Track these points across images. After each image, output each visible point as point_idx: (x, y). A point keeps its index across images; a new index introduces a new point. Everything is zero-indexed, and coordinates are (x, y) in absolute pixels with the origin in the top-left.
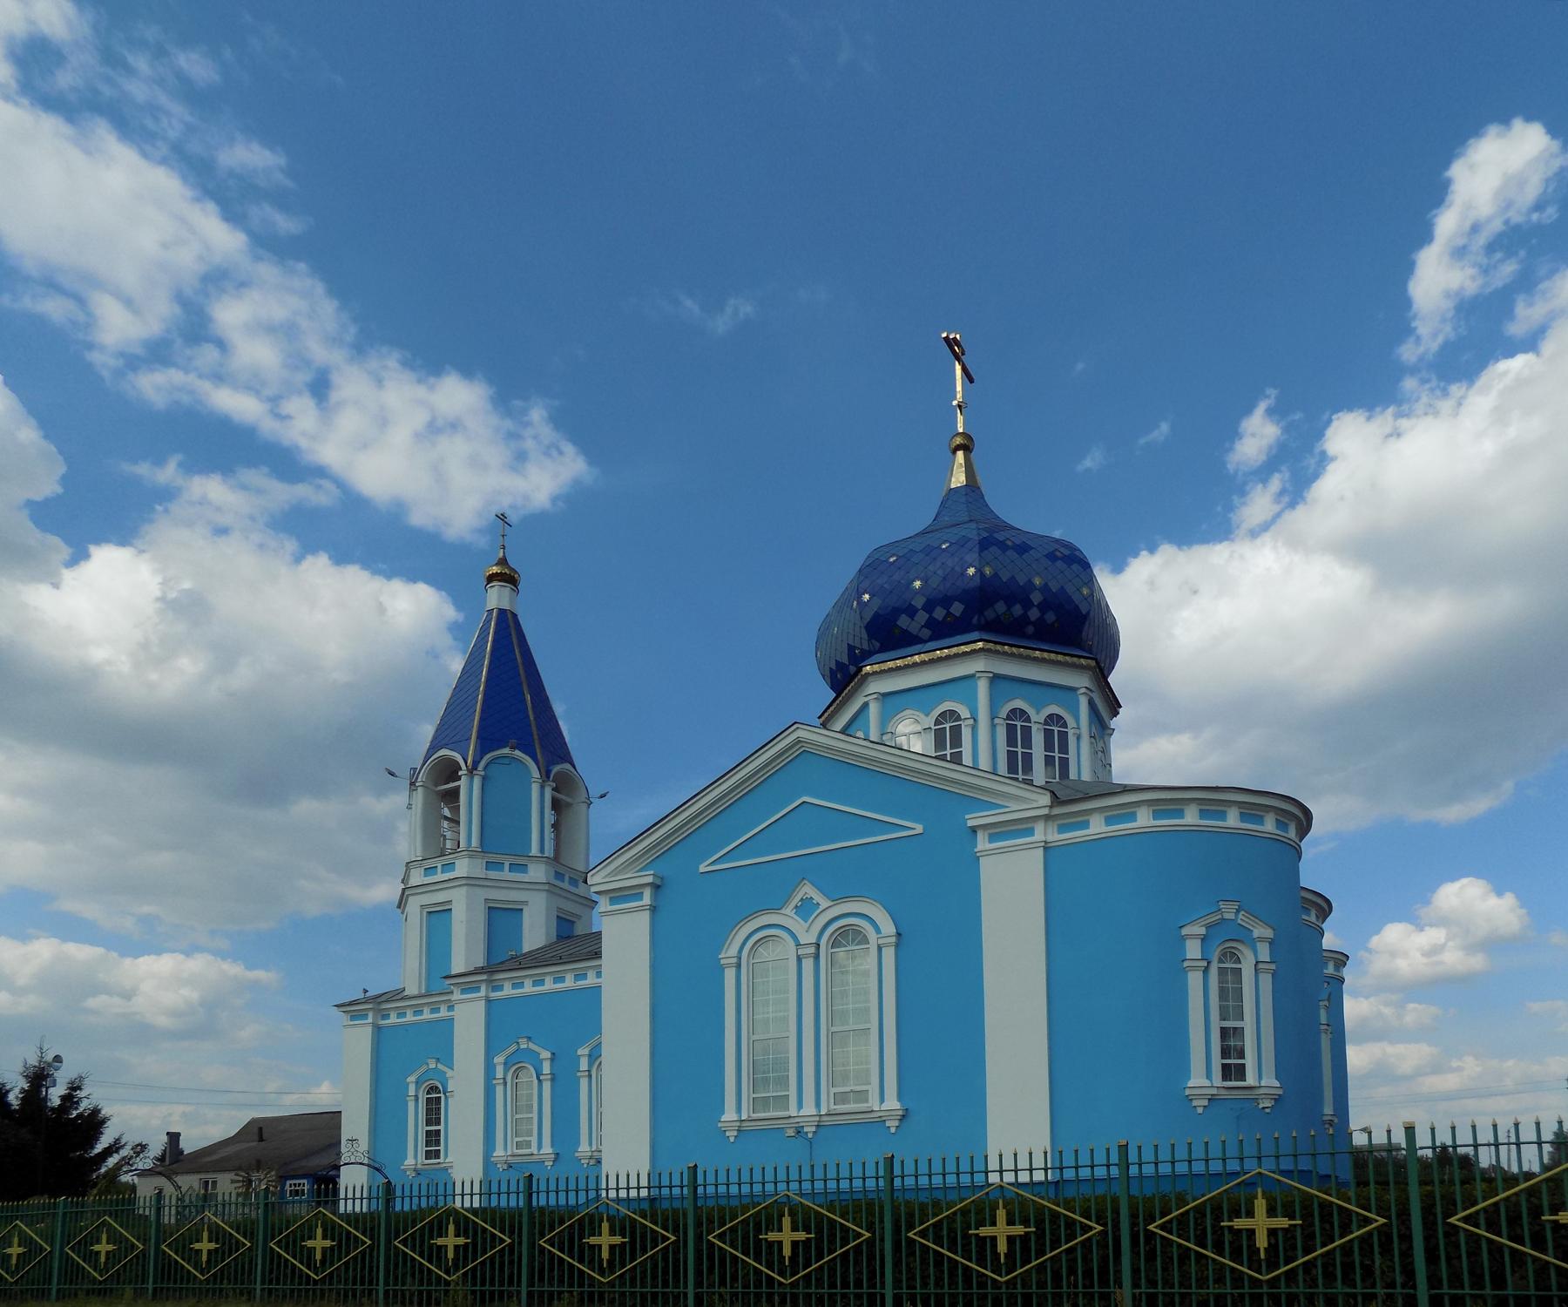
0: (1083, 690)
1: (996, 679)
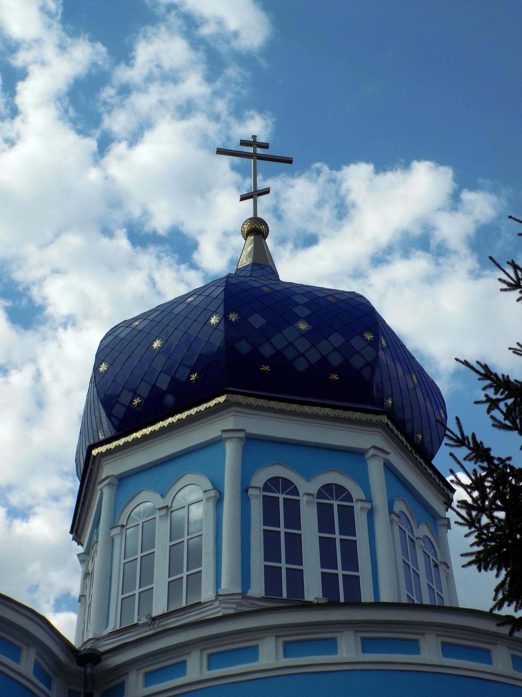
0: (372, 452)
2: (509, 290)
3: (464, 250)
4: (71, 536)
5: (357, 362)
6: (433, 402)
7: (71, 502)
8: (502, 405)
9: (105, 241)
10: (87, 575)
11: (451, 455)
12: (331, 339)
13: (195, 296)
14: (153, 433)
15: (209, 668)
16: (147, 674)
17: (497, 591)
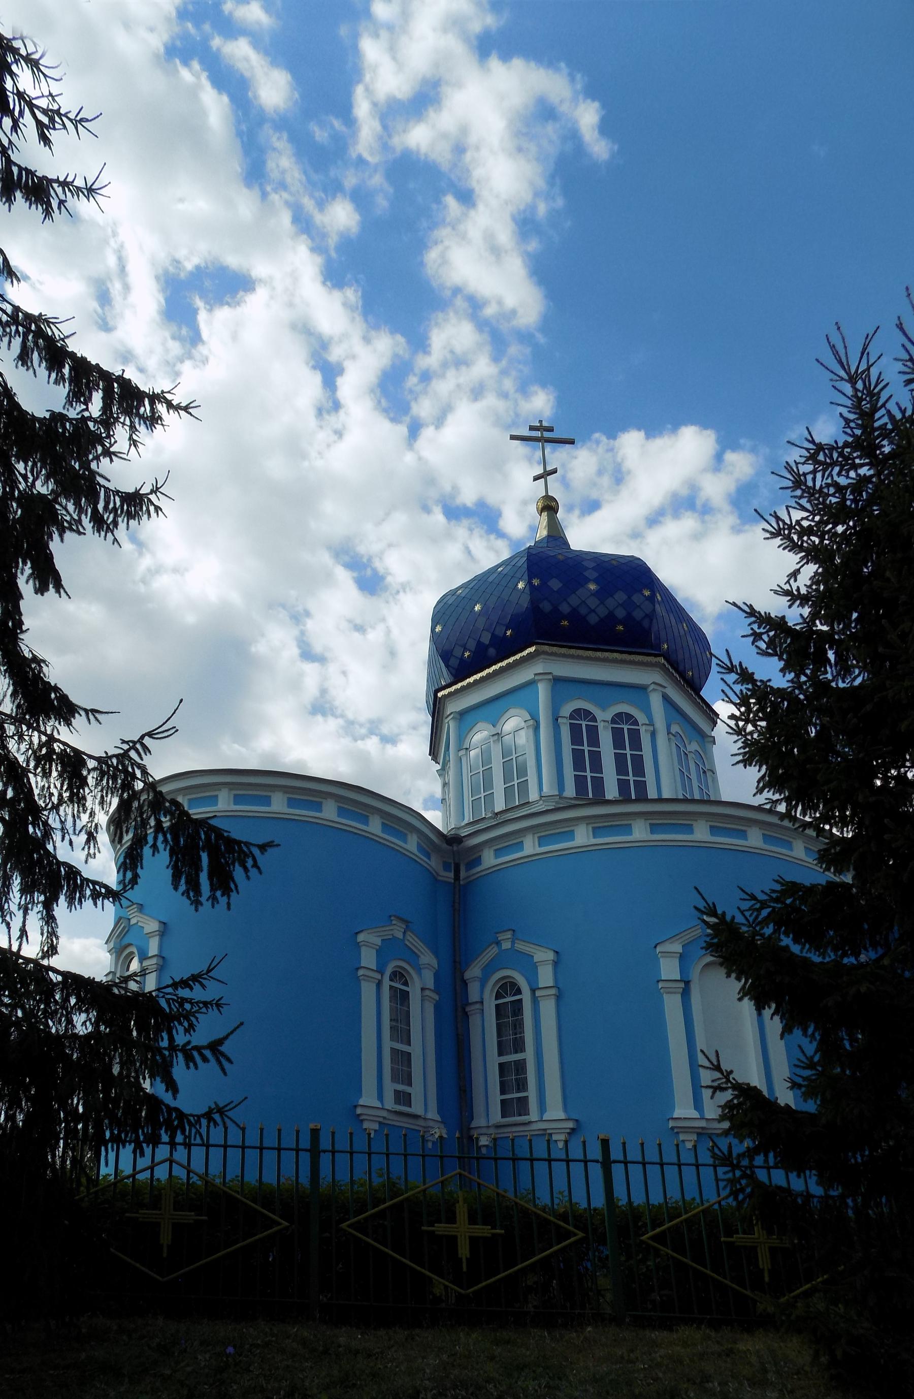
1: (557, 681)
2: (771, 538)
3: (727, 507)
4: (430, 757)
5: (638, 615)
6: (701, 645)
7: (427, 730)
8: (765, 637)
9: (425, 516)
10: (445, 785)
11: (722, 679)
12: (617, 596)
13: (504, 566)
14: (482, 678)
15: (540, 846)
16: (496, 850)
17: (759, 782)
